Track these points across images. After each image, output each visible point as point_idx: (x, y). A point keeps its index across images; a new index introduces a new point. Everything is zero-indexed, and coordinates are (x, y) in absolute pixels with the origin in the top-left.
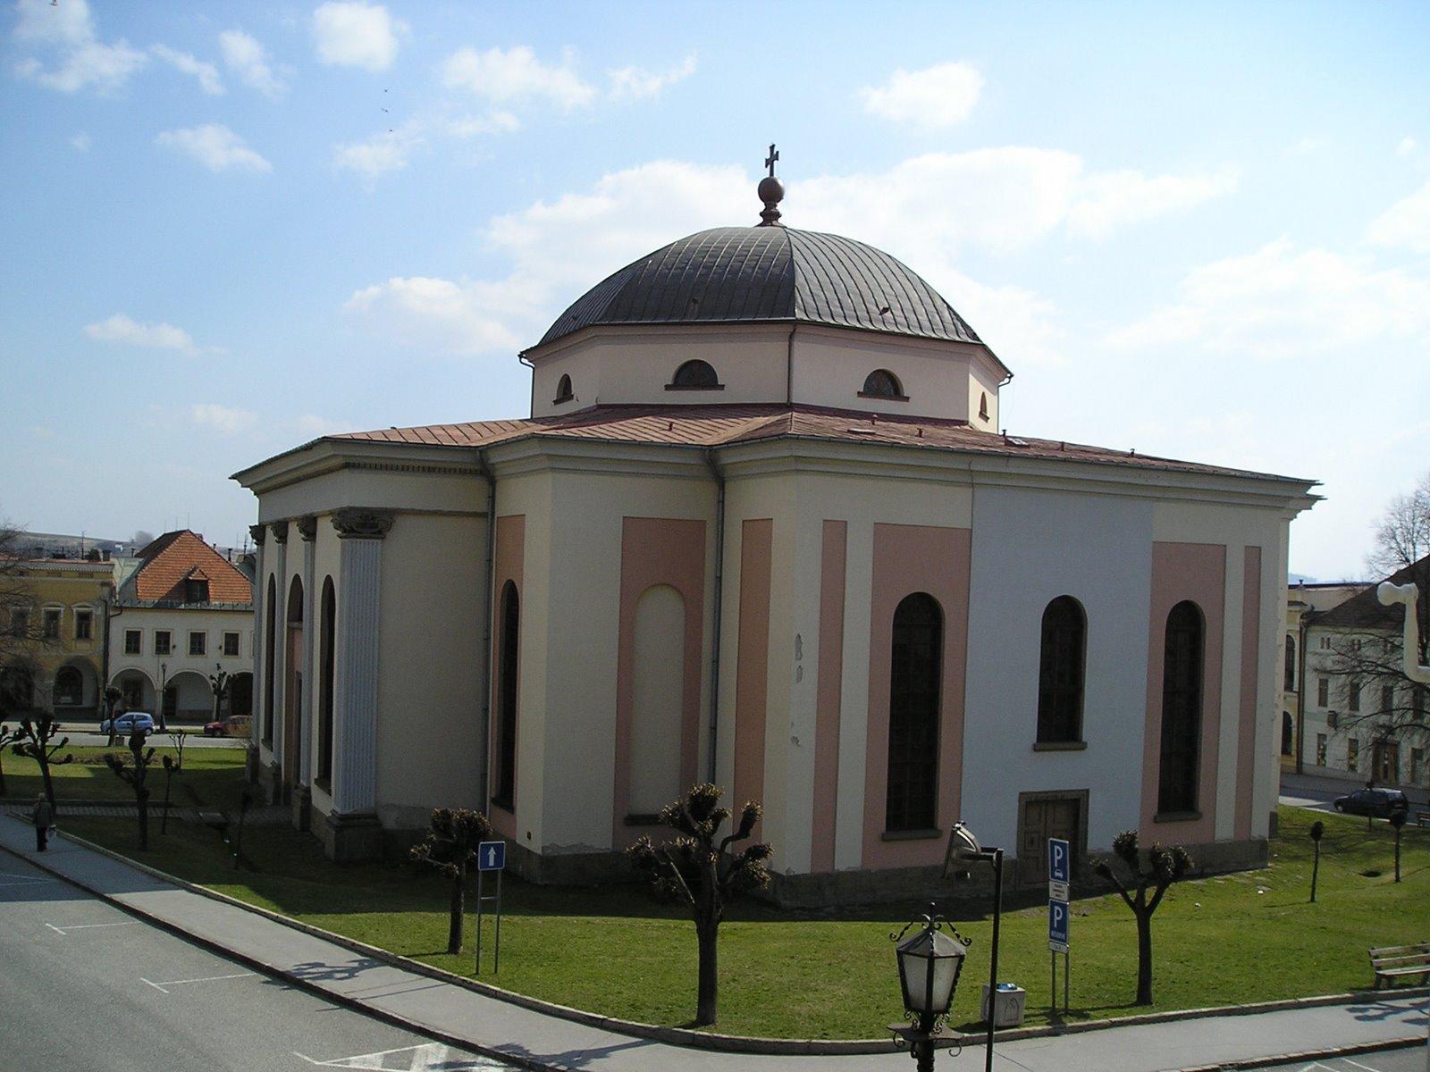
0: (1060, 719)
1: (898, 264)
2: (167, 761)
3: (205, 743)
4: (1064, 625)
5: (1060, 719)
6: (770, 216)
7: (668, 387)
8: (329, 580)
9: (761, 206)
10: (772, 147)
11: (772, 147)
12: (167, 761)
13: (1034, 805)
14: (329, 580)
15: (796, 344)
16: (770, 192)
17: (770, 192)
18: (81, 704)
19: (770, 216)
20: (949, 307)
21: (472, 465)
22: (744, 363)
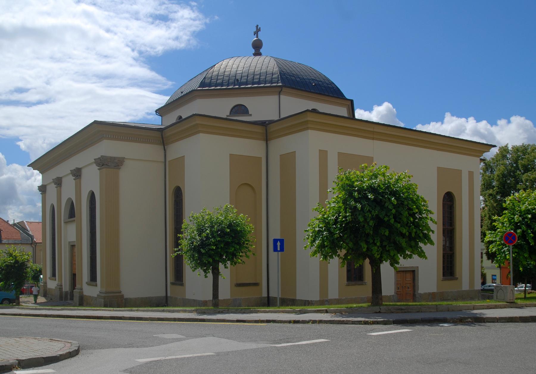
8: (92, 196)
14: (92, 196)
15: (282, 96)
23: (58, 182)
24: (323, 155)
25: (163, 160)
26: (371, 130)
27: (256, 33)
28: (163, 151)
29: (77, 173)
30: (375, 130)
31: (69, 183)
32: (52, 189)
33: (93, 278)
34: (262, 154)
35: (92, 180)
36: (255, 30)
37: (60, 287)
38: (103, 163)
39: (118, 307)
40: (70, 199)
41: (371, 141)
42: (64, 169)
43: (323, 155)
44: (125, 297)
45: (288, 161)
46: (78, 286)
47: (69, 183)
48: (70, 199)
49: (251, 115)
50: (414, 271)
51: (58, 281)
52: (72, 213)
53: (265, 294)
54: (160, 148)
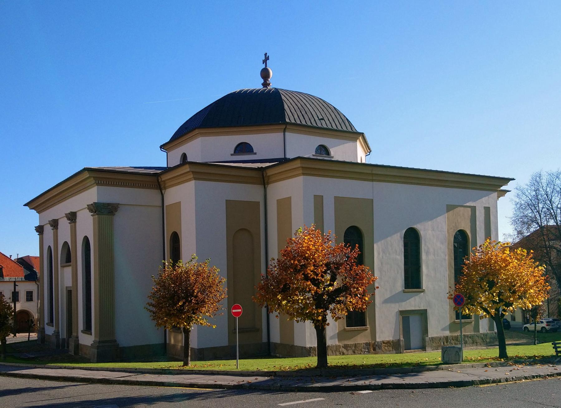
0: (413, 279)
1: (324, 101)
2: (284, 255)
3: (224, 380)
4: (412, 241)
5: (413, 279)
6: (265, 84)
7: (232, 155)
8: (86, 240)
9: (262, 81)
10: (266, 54)
11: (266, 54)
12: (284, 255)
13: (405, 317)
14: (86, 240)
15: (287, 134)
16: (265, 74)
17: (265, 74)
18: (191, 361)
19: (265, 84)
20: (347, 119)
21: (153, 180)
22: (266, 143)
23: (55, 224)
24: (319, 201)
25: (161, 205)
26: (370, 172)
27: (265, 62)
28: (160, 196)
29: (72, 217)
30: (374, 172)
31: (64, 224)
32: (48, 230)
33: (88, 329)
34: (261, 200)
35: (87, 225)
36: (264, 59)
37: (57, 334)
38: (96, 209)
39: (98, 361)
40: (66, 243)
41: (371, 183)
42: (59, 211)
43: (319, 201)
44: (121, 346)
45: (285, 205)
46: (74, 334)
47: (64, 224)
48: (66, 243)
49: (255, 154)
50: (425, 311)
51: (56, 328)
52: (68, 258)
53: (265, 340)
54: (158, 191)
